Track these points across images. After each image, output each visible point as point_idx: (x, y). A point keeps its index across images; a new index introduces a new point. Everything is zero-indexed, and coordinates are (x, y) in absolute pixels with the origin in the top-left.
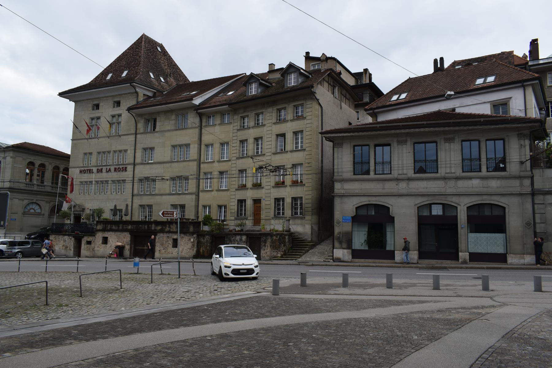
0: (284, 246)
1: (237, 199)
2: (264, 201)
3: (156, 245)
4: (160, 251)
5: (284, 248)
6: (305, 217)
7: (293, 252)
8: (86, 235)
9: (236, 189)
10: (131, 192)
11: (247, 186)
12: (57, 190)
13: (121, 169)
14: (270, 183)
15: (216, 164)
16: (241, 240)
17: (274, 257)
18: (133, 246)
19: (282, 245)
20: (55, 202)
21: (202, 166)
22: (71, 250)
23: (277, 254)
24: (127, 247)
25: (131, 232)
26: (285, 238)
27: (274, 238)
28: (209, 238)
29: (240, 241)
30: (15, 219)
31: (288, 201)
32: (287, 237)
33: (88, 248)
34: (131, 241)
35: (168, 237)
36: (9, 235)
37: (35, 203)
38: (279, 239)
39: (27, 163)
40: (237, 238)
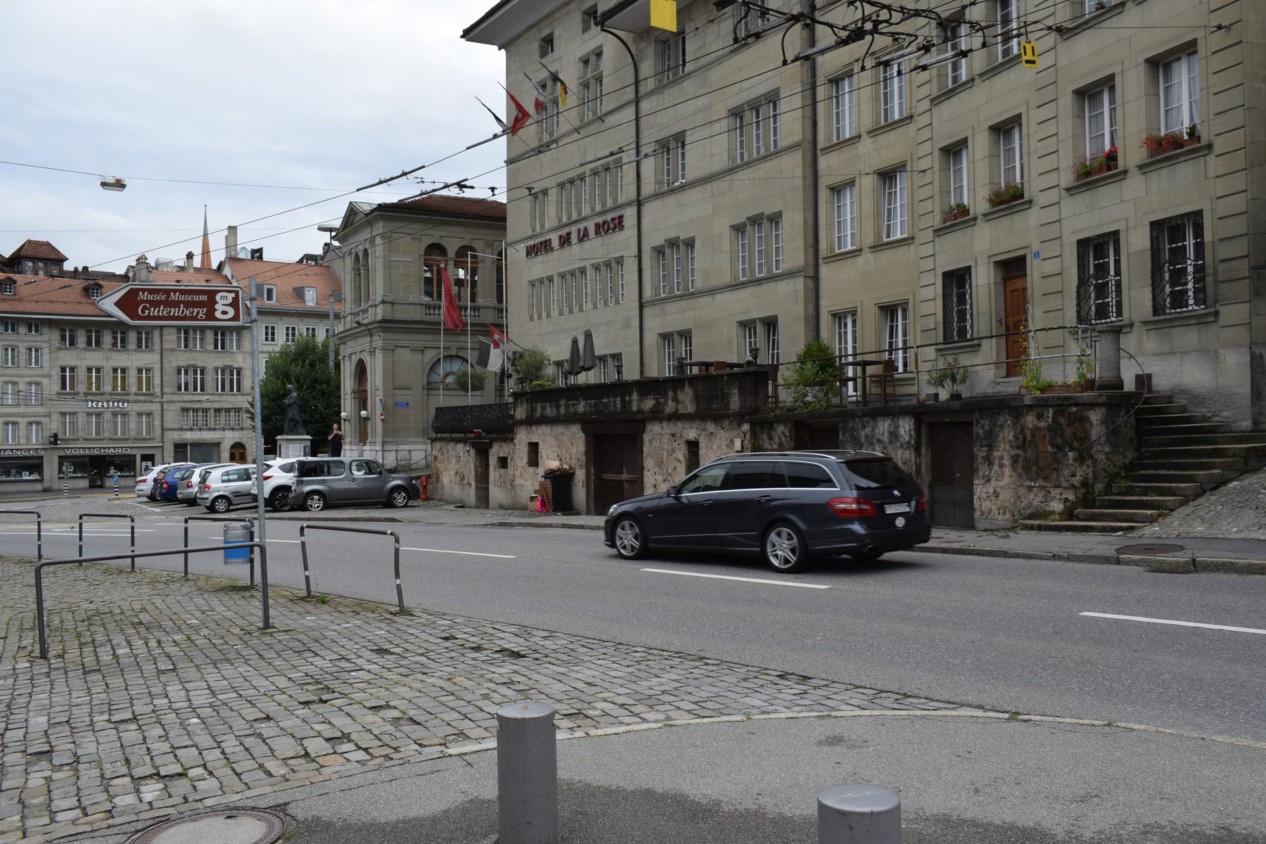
0: (1081, 459)
1: (940, 272)
2: (1037, 262)
3: (645, 464)
4: (655, 486)
5: (1082, 472)
6: (1217, 314)
7: (1129, 491)
8: (496, 440)
9: (935, 231)
10: (637, 297)
11: (972, 211)
12: (439, 315)
13: (611, 226)
14: (1055, 174)
15: (866, 145)
16: (894, 435)
17: (1031, 517)
18: (592, 470)
19: (1071, 455)
20: (437, 351)
21: (823, 162)
22: (469, 484)
23: (1047, 498)
24: (580, 475)
25: (586, 423)
26: (1084, 420)
27: (1030, 420)
28: (787, 434)
29: (891, 442)
30: (408, 404)
31: (1137, 241)
32: (1095, 416)
33: (502, 479)
34: (587, 453)
35: (673, 435)
36: (394, 448)
37: (457, 356)
38: (1055, 428)
39: (423, 249)
40: (881, 428)
